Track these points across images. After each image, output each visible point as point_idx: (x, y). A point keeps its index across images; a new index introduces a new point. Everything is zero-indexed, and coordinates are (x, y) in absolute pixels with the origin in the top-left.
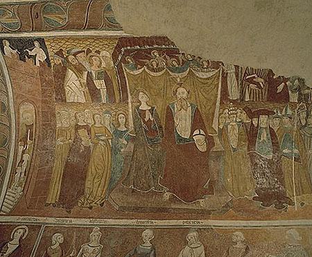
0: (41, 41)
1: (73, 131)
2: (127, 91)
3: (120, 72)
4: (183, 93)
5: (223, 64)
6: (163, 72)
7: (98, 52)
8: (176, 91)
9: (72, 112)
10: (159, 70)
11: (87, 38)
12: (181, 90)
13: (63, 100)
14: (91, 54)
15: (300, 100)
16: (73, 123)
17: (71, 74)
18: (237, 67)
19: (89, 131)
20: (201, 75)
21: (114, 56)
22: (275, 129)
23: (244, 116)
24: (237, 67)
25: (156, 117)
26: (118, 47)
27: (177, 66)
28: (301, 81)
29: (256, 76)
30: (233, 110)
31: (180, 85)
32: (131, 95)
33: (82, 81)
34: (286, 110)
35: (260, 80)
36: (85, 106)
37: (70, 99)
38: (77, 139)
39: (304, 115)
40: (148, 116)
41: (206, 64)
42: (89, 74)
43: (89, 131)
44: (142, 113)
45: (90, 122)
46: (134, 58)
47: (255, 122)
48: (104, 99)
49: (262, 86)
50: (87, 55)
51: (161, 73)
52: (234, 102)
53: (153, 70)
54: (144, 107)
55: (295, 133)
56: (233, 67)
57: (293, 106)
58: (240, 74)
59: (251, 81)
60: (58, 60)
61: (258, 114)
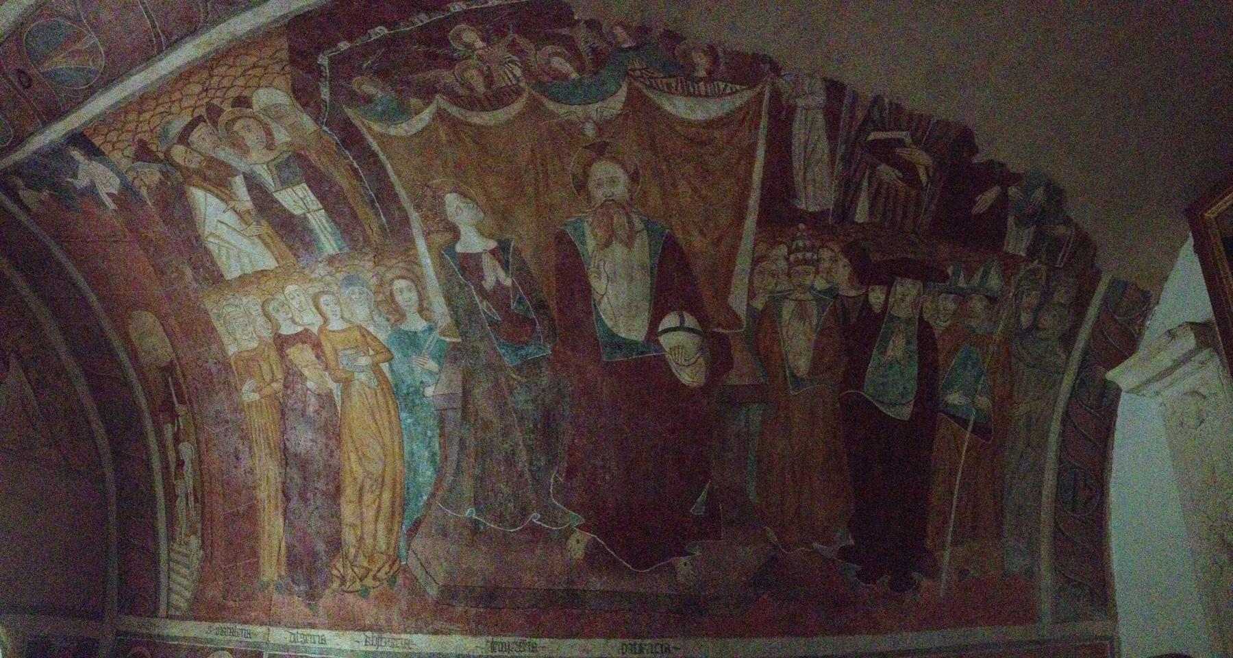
0: (78, 139)
1: (273, 354)
2: (392, 186)
3: (350, 138)
4: (613, 181)
5: (776, 69)
6: (517, 107)
7: (242, 102)
8: (586, 175)
9: (251, 301)
10: (498, 99)
11: (185, 75)
12: (603, 170)
13: (216, 279)
14: (223, 119)
15: (1032, 252)
16: (266, 334)
17: (204, 202)
18: (835, 89)
19: (317, 346)
20: (681, 107)
21: (303, 95)
22: (940, 326)
23: (843, 273)
24: (835, 89)
25: (522, 273)
26: (301, 58)
27: (574, 75)
28: (1055, 194)
29: (908, 140)
30: (805, 249)
31: (600, 150)
32: (418, 207)
33: (239, 207)
34: (986, 273)
35: (922, 159)
36: (283, 275)
37: (232, 272)
38: (292, 376)
39: (1032, 299)
40: (494, 275)
41: (702, 63)
42: (253, 184)
43: (317, 346)
44: (469, 266)
45: (310, 320)
46: (383, 73)
47: (877, 297)
48: (329, 243)
49: (924, 178)
50: (215, 123)
51: (501, 115)
52: (815, 220)
53: (474, 103)
54: (473, 242)
55: (993, 348)
56: (819, 85)
57: (1010, 265)
58: (845, 116)
59: (885, 151)
60: (151, 175)
61: (887, 275)
